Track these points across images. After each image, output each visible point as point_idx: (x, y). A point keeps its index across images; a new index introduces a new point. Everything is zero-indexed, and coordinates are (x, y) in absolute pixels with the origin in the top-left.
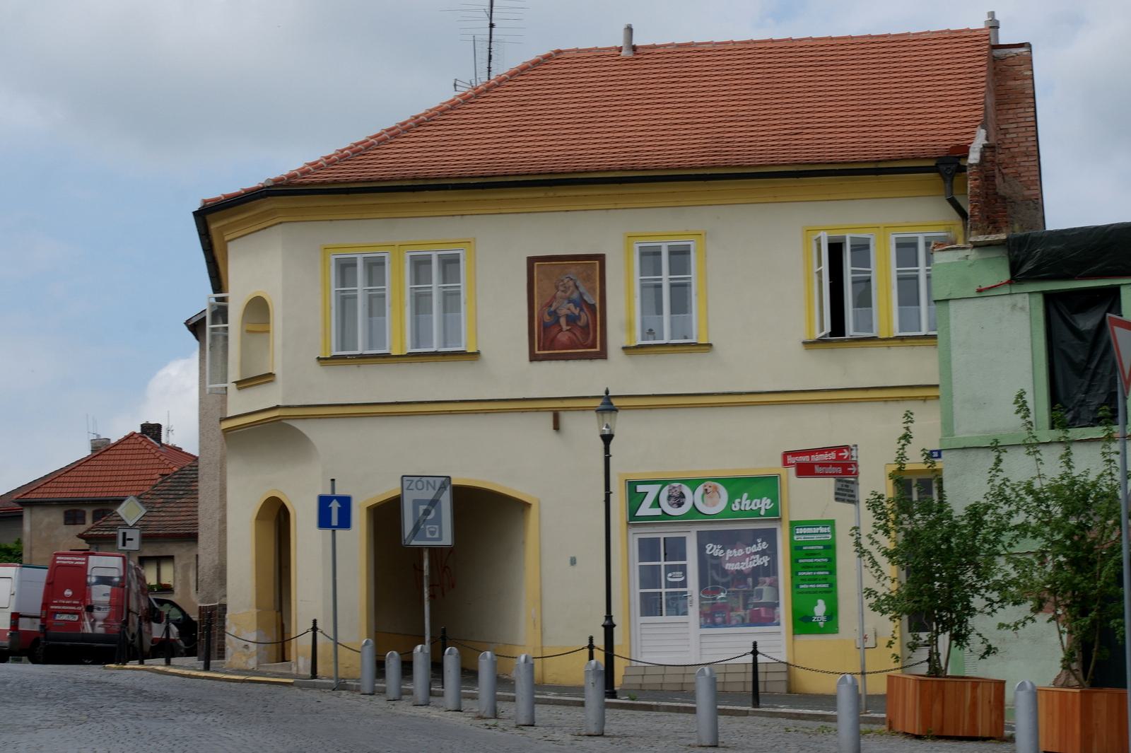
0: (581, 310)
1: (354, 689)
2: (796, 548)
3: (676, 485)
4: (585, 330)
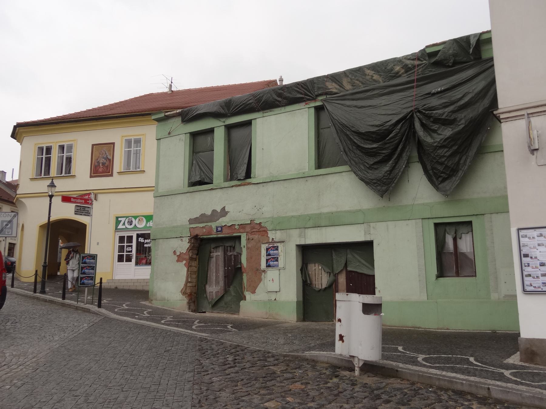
0: (107, 161)
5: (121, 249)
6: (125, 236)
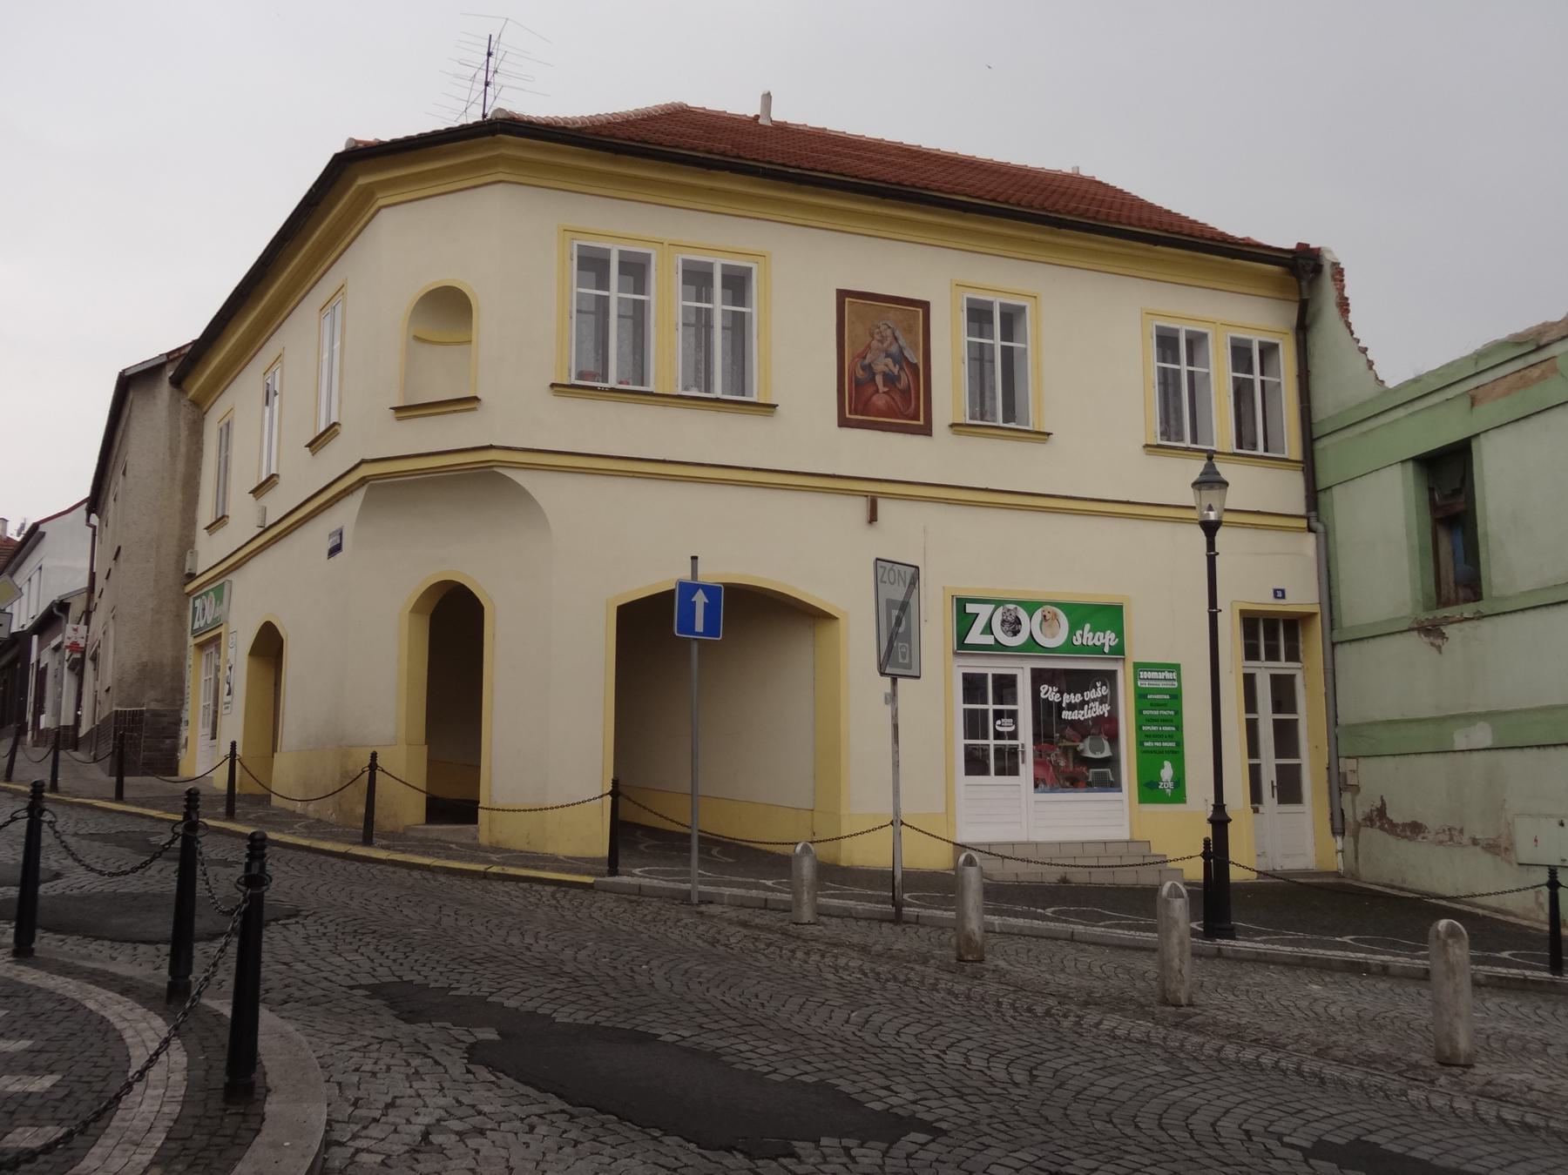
0: (901, 368)
2: (1141, 695)
4: (906, 394)
5: (974, 724)
6: (986, 675)
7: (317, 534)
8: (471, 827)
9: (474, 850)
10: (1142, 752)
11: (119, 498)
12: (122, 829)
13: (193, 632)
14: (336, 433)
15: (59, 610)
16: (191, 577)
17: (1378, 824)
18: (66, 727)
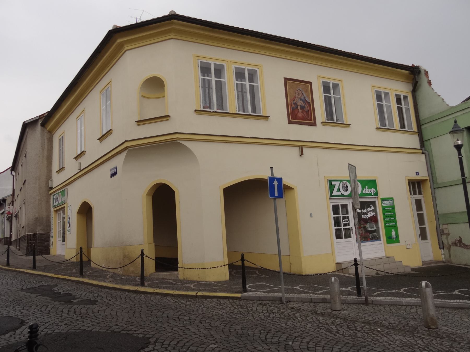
0: (305, 104)
1: (295, 300)
2: (384, 208)
3: (345, 182)
4: (307, 112)
5: (337, 222)
7: (107, 168)
8: (175, 273)
9: (186, 283)
10: (386, 227)
11: (23, 165)
12: (40, 284)
13: (53, 206)
14: (111, 133)
15: (3, 202)
16: (51, 188)
17: (459, 245)
18: (7, 238)
